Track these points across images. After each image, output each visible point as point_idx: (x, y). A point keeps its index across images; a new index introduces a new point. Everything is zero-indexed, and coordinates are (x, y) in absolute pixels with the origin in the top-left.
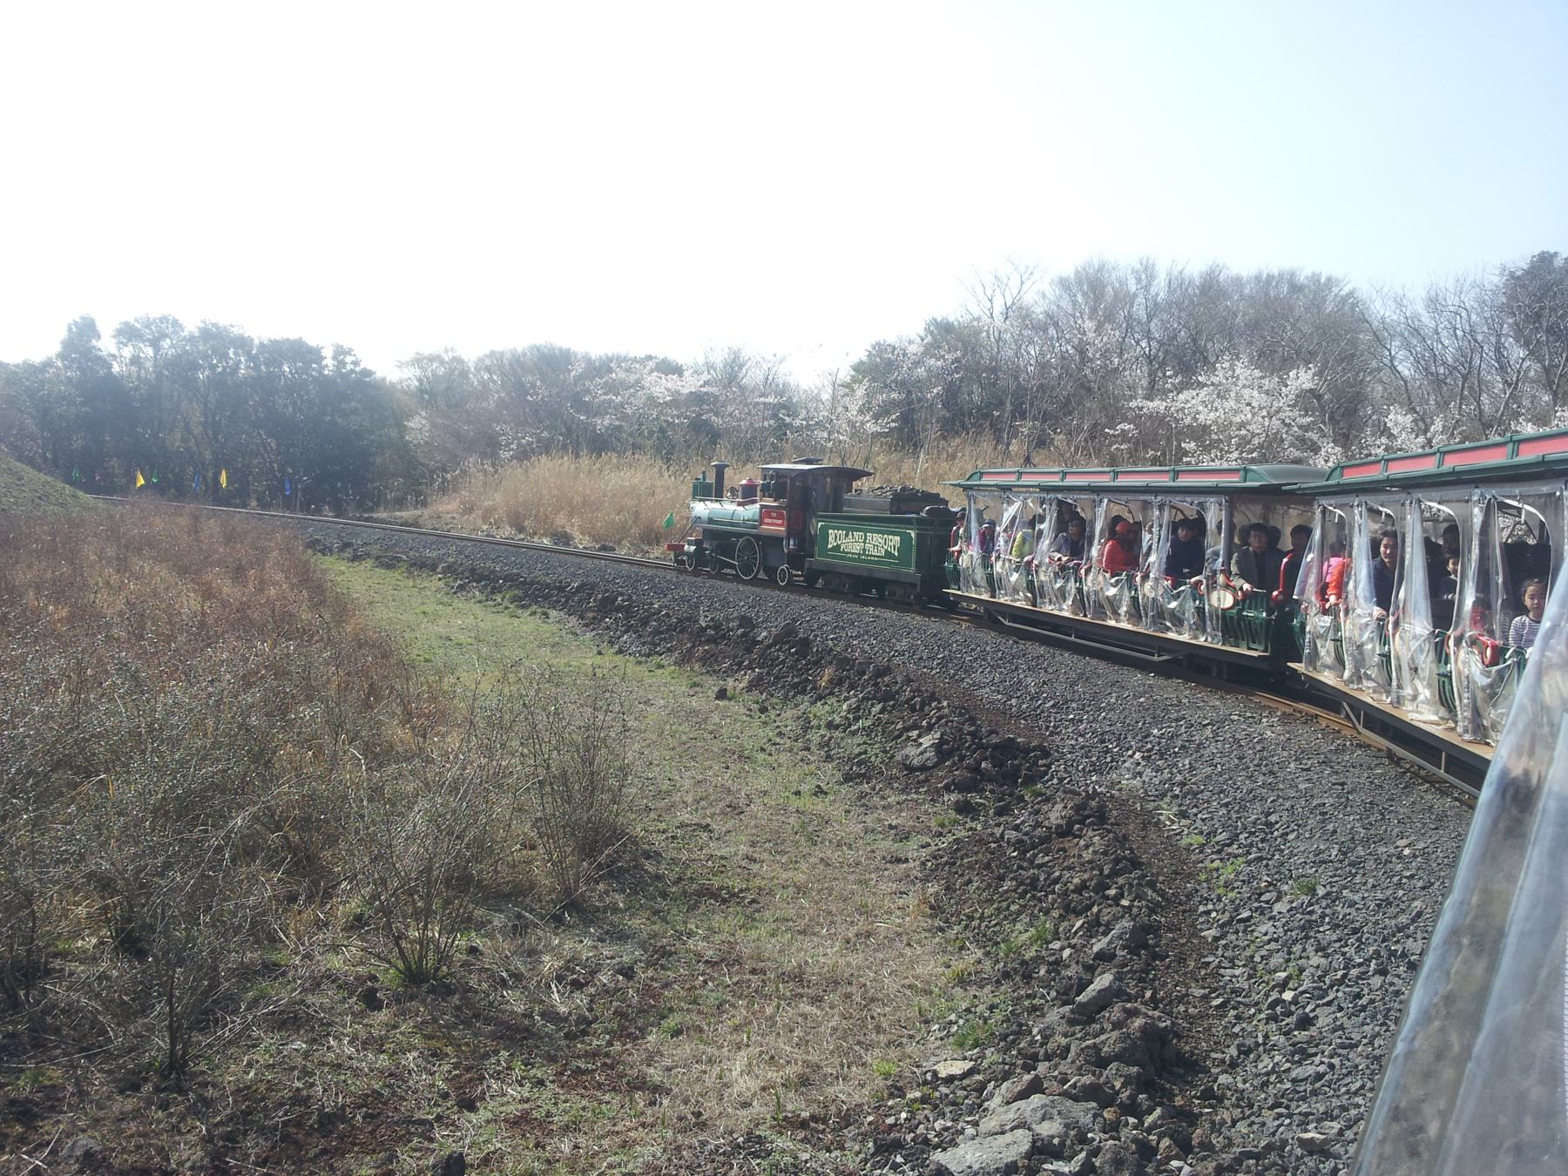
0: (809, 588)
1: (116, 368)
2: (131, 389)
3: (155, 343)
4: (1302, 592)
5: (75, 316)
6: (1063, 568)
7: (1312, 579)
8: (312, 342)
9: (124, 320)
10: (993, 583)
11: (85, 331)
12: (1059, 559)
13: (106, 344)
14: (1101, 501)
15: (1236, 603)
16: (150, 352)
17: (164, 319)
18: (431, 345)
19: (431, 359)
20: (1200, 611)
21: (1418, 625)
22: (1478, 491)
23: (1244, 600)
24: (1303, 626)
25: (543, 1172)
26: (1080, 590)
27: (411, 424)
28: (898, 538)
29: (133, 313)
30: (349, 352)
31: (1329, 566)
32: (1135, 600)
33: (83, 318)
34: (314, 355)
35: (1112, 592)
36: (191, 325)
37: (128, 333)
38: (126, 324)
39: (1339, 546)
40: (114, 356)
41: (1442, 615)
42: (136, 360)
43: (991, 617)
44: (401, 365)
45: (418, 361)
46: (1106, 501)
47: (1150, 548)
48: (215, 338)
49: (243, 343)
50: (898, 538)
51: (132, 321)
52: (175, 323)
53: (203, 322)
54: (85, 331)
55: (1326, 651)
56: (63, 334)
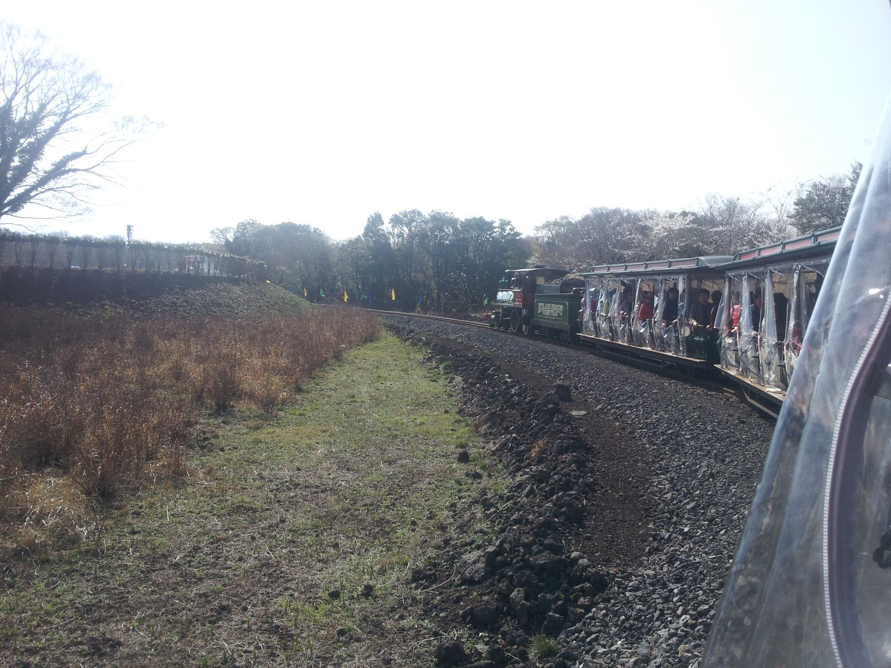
0: (531, 335)
1: (392, 241)
2: (396, 250)
3: (408, 225)
4: (719, 324)
5: (371, 213)
6: (624, 318)
7: (724, 317)
8: (488, 219)
9: (394, 214)
10: (597, 328)
11: (376, 220)
12: (622, 314)
13: (387, 227)
14: (638, 280)
15: (691, 333)
16: (406, 229)
17: (413, 212)
18: (554, 216)
19: (556, 223)
20: (677, 338)
21: (771, 339)
22: (795, 264)
23: (694, 331)
24: (721, 343)
25: (401, 665)
26: (630, 330)
27: (529, 261)
28: (562, 306)
29: (397, 210)
30: (509, 223)
31: (734, 310)
32: (651, 334)
33: (375, 214)
34: (489, 226)
35: (642, 331)
36: (426, 212)
37: (396, 221)
38: (396, 216)
39: (736, 296)
40: (390, 233)
41: (781, 335)
42: (400, 235)
43: (592, 346)
44: (537, 229)
45: (547, 226)
46: (640, 280)
47: (657, 305)
48: (439, 220)
49: (452, 222)
50: (562, 306)
51: (398, 214)
52: (419, 214)
53: (433, 211)
54: (376, 220)
55: (731, 357)
56: (365, 223)
